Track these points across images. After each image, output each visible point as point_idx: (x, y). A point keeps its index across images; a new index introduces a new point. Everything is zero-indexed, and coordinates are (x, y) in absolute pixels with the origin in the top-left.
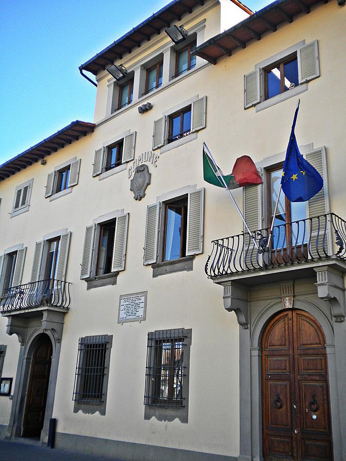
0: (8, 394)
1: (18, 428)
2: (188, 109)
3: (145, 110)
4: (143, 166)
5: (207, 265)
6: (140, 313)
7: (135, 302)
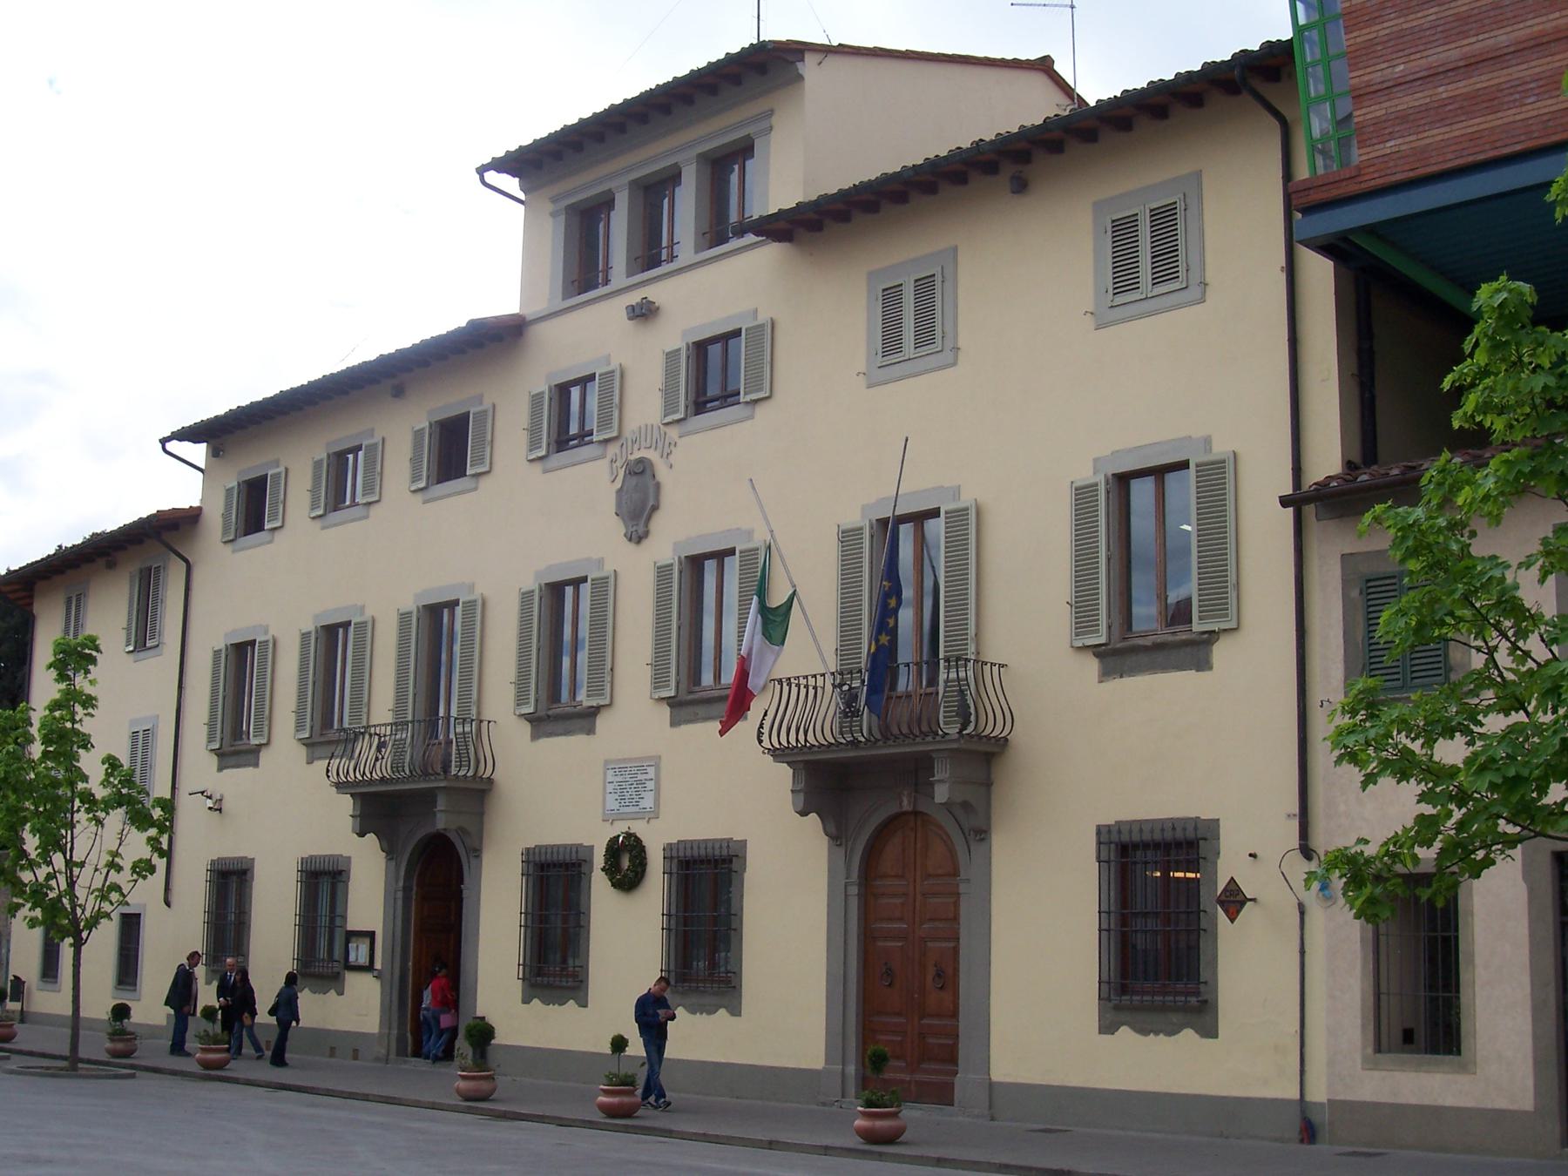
0: (369, 968)
1: (401, 1039)
2: (737, 333)
3: (644, 313)
4: (641, 461)
5: (761, 726)
6: (648, 802)
7: (635, 777)
